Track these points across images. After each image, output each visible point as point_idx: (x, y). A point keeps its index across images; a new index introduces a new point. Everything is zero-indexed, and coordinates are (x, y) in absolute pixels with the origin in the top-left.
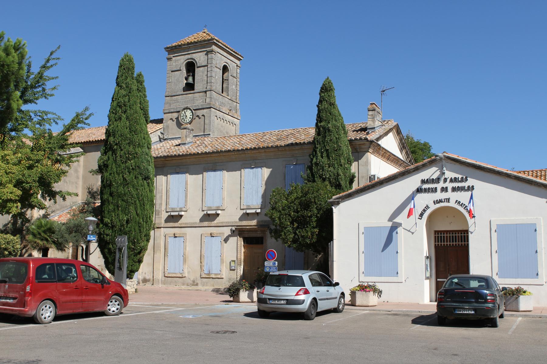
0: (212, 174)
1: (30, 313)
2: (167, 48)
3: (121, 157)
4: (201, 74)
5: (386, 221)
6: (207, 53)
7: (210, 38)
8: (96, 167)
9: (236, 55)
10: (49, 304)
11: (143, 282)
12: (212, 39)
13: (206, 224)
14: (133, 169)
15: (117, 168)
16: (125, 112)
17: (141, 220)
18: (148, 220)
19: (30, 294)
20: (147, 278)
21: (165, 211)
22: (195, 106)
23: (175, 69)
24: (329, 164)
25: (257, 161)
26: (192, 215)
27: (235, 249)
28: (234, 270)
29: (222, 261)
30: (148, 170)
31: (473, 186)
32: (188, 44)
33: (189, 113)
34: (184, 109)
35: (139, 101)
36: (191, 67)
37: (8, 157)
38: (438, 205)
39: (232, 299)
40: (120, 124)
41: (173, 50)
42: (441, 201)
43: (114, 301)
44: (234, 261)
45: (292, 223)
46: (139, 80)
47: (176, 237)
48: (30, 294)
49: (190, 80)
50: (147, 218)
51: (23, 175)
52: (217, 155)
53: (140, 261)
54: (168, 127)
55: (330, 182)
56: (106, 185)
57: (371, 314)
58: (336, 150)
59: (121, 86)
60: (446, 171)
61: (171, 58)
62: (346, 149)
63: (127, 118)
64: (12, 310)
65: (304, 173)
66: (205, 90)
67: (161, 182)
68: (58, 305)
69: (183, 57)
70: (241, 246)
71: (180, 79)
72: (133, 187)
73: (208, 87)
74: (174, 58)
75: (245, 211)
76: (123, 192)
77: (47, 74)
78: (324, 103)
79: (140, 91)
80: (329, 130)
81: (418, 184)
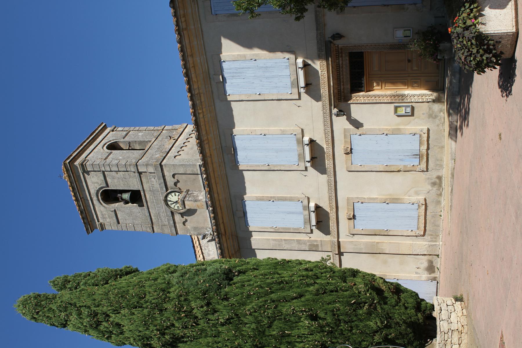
3: (186, 327)
4: (116, 181)
6: (86, 172)
9: (97, 132)
13: (328, 163)
14: (208, 304)
15: (206, 336)
16: (108, 316)
17: (312, 288)
18: (314, 272)
20: (426, 264)
21: (310, 235)
22: (161, 188)
23: (115, 218)
25: (212, 72)
26: (314, 187)
27: (375, 107)
28: (413, 108)
29: (396, 132)
30: (213, 274)
34: (167, 205)
36: (110, 196)
41: (89, 221)
44: (396, 108)
47: (354, 216)
49: (126, 196)
50: (307, 277)
52: (206, 146)
53: (398, 289)
54: (195, 229)
61: (101, 224)
63: (116, 311)
69: (96, 208)
70: (368, 96)
71: (127, 212)
72: (244, 304)
73: (133, 170)
74: (101, 221)
75: (302, 91)
76: (253, 326)
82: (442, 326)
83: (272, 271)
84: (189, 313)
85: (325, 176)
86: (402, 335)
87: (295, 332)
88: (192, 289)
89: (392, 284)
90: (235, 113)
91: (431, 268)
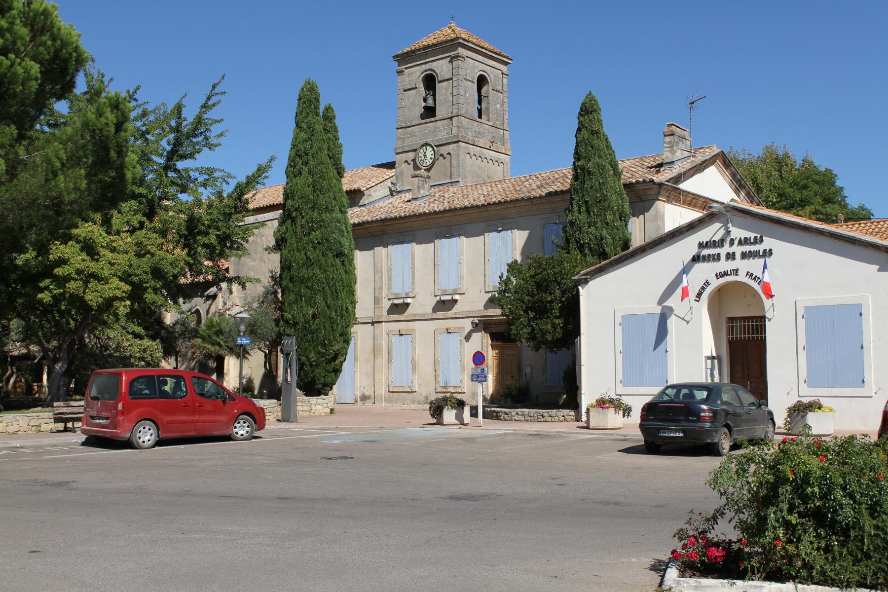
0: (445, 241)
1: (123, 435)
2: (397, 56)
4: (444, 91)
5: (655, 304)
7: (453, 36)
8: (272, 243)
10: (148, 424)
11: (362, 400)
12: (457, 38)
13: (440, 314)
14: (319, 243)
16: (307, 163)
17: (334, 314)
19: (123, 413)
20: (367, 394)
22: (438, 141)
23: (409, 87)
24: (589, 223)
25: (505, 221)
26: (422, 304)
31: (770, 250)
32: (425, 48)
33: (429, 152)
34: (423, 146)
35: (325, 146)
36: (430, 82)
37: (114, 244)
38: (723, 280)
39: (435, 421)
40: (300, 181)
41: (404, 59)
42: (725, 274)
43: (242, 422)
45: (526, 312)
46: (329, 116)
47: (401, 335)
48: (123, 413)
51: (131, 266)
54: (402, 173)
55: (591, 250)
56: (286, 266)
57: (505, 434)
58: (599, 202)
59: (301, 127)
60: (732, 228)
61: (403, 71)
62: (619, 200)
63: (310, 172)
64: (104, 432)
65: (558, 238)
66: (450, 115)
67: (363, 261)
68: (160, 426)
71: (416, 100)
72: (320, 268)
73: (454, 111)
74: (406, 71)
76: (306, 276)
77: (210, 115)
78: (584, 131)
79: (329, 131)
80: (589, 173)
81: (695, 251)
82: (314, 400)
83: (345, 284)
84: (312, 229)
85: (431, 311)
86: (306, 374)
87: (304, 304)
88: (329, 229)
89: (341, 367)
90: (476, 238)
91: (364, 398)
